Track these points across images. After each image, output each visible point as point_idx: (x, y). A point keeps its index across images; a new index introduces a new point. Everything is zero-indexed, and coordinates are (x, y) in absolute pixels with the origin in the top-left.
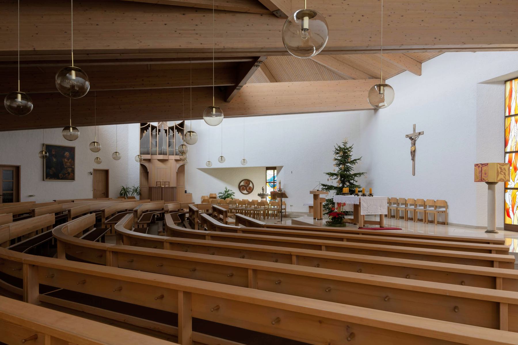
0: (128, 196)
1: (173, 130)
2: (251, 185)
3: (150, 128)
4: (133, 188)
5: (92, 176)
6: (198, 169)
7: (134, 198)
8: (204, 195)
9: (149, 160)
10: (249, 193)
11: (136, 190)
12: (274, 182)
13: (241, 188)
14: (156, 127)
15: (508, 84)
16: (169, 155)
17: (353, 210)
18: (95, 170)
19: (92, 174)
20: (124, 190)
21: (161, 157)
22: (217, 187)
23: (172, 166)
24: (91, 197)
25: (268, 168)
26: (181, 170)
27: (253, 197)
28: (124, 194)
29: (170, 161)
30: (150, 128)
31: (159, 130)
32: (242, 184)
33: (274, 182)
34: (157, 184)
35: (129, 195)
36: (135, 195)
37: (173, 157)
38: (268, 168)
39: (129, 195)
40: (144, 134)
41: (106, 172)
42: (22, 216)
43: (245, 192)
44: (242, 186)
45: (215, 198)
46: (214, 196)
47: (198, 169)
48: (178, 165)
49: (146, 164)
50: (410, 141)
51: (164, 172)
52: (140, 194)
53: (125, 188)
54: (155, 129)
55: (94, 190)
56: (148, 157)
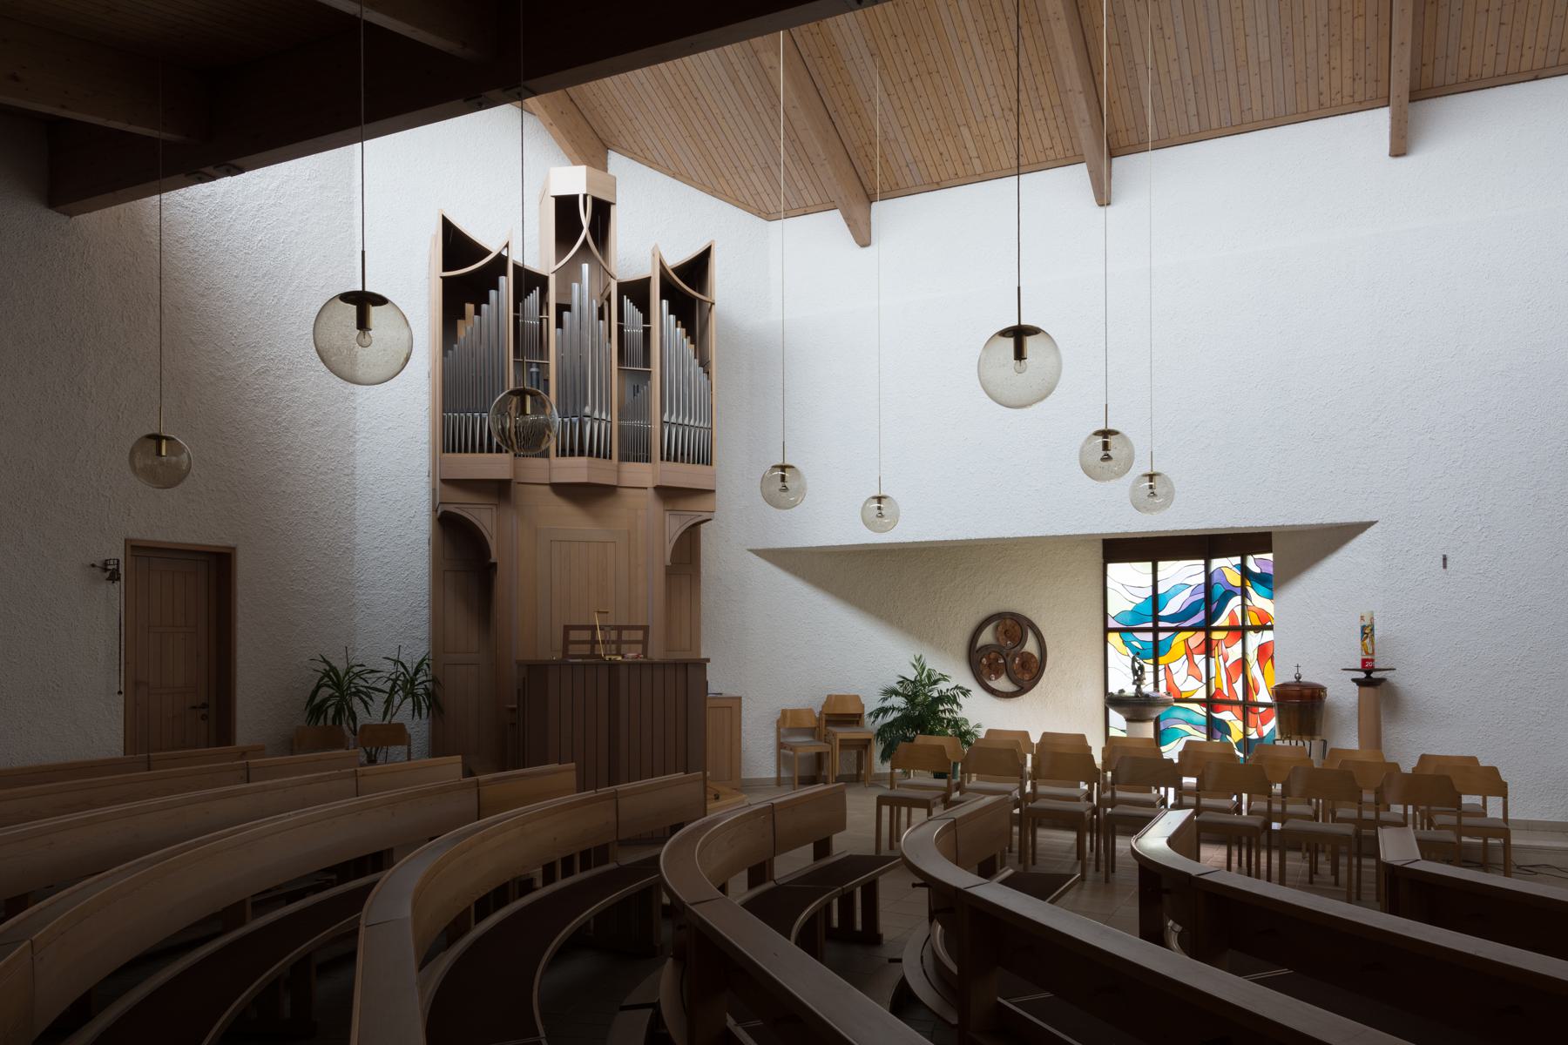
0: (363, 718)
1: (643, 305)
2: (1031, 646)
3: (507, 283)
4: (389, 667)
5: (116, 590)
6: (758, 552)
7: (397, 734)
8: (791, 704)
9: (499, 491)
10: (1022, 690)
11: (405, 684)
12: (1156, 630)
13: (983, 664)
14: (542, 281)
15: (1501, 70)
16: (624, 458)
17: (458, 758)
18: (139, 550)
19: (114, 577)
20: (338, 685)
21: (576, 469)
22: (868, 660)
23: (642, 522)
24: (103, 735)
25: (1120, 549)
26: (686, 556)
27: (1031, 717)
28: (331, 709)
29: (630, 499)
30: (507, 283)
31: (562, 308)
32: (987, 637)
33: (1156, 630)
34: (567, 641)
35: (370, 714)
36: (404, 713)
37: (642, 475)
38: (1120, 549)
39: (370, 714)
40: (464, 329)
41: (217, 566)
42: (1354, 882)
43: (1002, 684)
44: (986, 647)
45: (854, 719)
46: (852, 710)
47: (758, 552)
48: (675, 527)
49: (482, 516)
50: (352, 309)
51: (576, 569)
52: (435, 703)
53: (341, 667)
54: (535, 296)
55: (135, 688)
56: (495, 465)
